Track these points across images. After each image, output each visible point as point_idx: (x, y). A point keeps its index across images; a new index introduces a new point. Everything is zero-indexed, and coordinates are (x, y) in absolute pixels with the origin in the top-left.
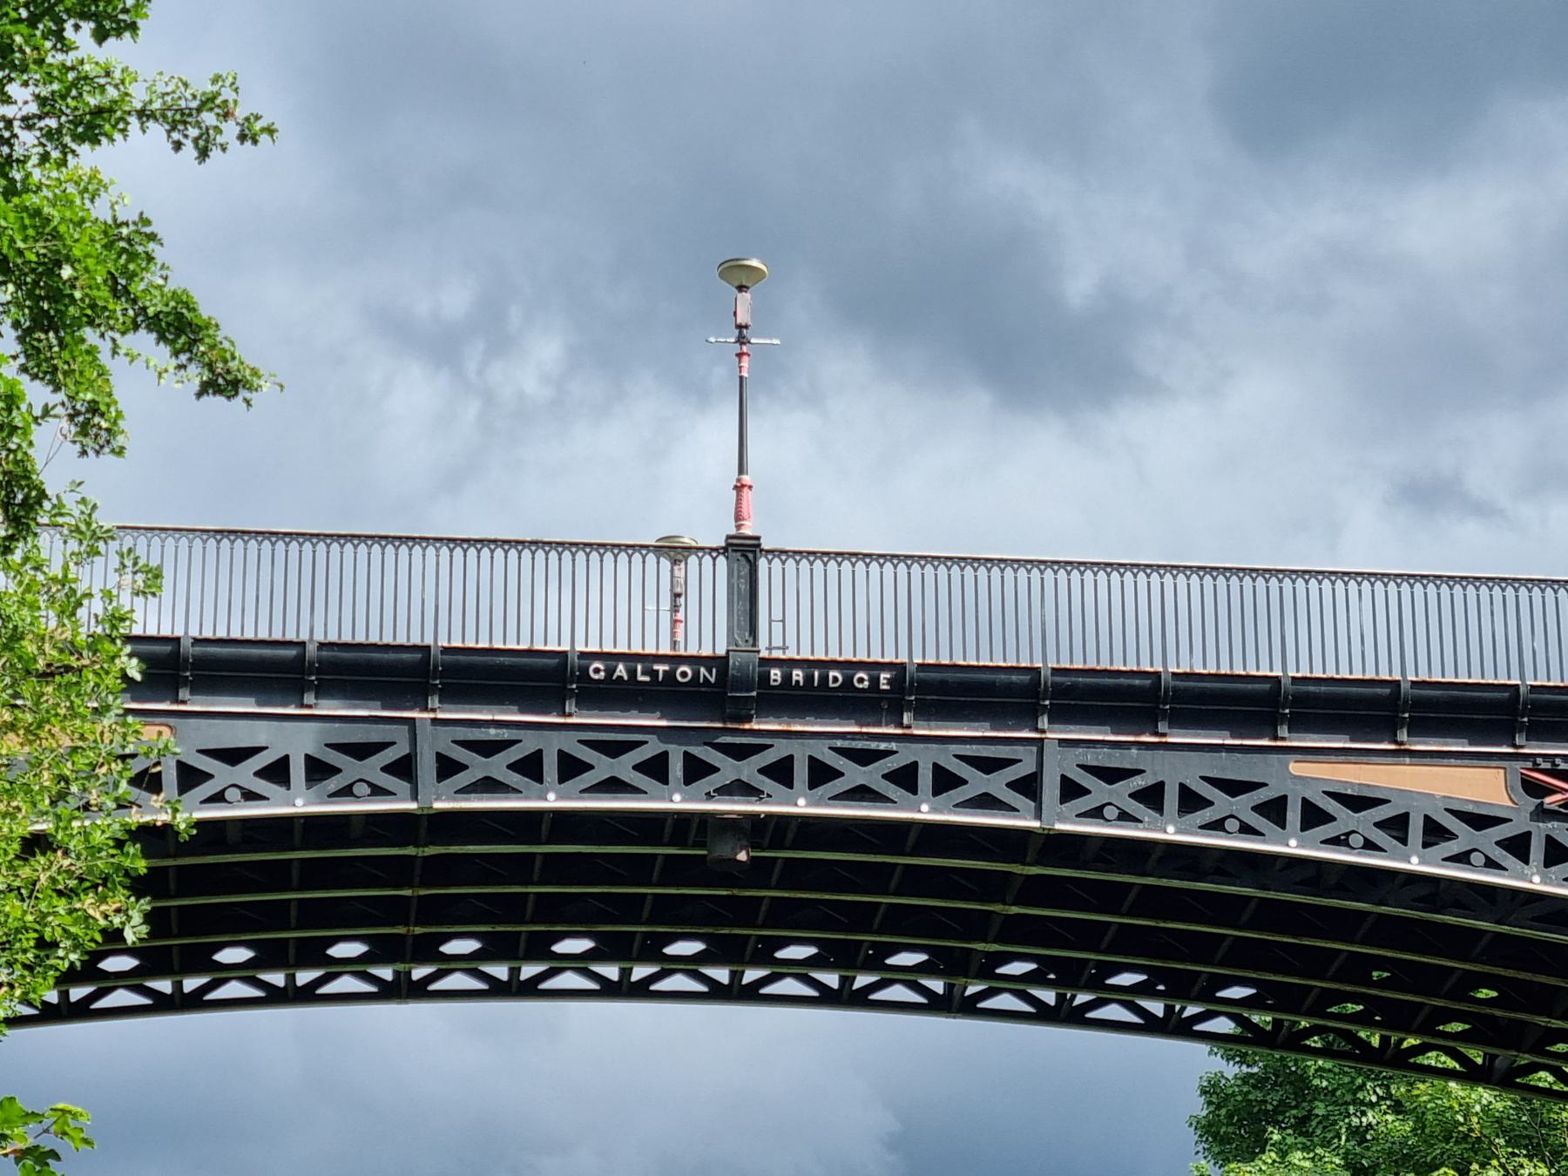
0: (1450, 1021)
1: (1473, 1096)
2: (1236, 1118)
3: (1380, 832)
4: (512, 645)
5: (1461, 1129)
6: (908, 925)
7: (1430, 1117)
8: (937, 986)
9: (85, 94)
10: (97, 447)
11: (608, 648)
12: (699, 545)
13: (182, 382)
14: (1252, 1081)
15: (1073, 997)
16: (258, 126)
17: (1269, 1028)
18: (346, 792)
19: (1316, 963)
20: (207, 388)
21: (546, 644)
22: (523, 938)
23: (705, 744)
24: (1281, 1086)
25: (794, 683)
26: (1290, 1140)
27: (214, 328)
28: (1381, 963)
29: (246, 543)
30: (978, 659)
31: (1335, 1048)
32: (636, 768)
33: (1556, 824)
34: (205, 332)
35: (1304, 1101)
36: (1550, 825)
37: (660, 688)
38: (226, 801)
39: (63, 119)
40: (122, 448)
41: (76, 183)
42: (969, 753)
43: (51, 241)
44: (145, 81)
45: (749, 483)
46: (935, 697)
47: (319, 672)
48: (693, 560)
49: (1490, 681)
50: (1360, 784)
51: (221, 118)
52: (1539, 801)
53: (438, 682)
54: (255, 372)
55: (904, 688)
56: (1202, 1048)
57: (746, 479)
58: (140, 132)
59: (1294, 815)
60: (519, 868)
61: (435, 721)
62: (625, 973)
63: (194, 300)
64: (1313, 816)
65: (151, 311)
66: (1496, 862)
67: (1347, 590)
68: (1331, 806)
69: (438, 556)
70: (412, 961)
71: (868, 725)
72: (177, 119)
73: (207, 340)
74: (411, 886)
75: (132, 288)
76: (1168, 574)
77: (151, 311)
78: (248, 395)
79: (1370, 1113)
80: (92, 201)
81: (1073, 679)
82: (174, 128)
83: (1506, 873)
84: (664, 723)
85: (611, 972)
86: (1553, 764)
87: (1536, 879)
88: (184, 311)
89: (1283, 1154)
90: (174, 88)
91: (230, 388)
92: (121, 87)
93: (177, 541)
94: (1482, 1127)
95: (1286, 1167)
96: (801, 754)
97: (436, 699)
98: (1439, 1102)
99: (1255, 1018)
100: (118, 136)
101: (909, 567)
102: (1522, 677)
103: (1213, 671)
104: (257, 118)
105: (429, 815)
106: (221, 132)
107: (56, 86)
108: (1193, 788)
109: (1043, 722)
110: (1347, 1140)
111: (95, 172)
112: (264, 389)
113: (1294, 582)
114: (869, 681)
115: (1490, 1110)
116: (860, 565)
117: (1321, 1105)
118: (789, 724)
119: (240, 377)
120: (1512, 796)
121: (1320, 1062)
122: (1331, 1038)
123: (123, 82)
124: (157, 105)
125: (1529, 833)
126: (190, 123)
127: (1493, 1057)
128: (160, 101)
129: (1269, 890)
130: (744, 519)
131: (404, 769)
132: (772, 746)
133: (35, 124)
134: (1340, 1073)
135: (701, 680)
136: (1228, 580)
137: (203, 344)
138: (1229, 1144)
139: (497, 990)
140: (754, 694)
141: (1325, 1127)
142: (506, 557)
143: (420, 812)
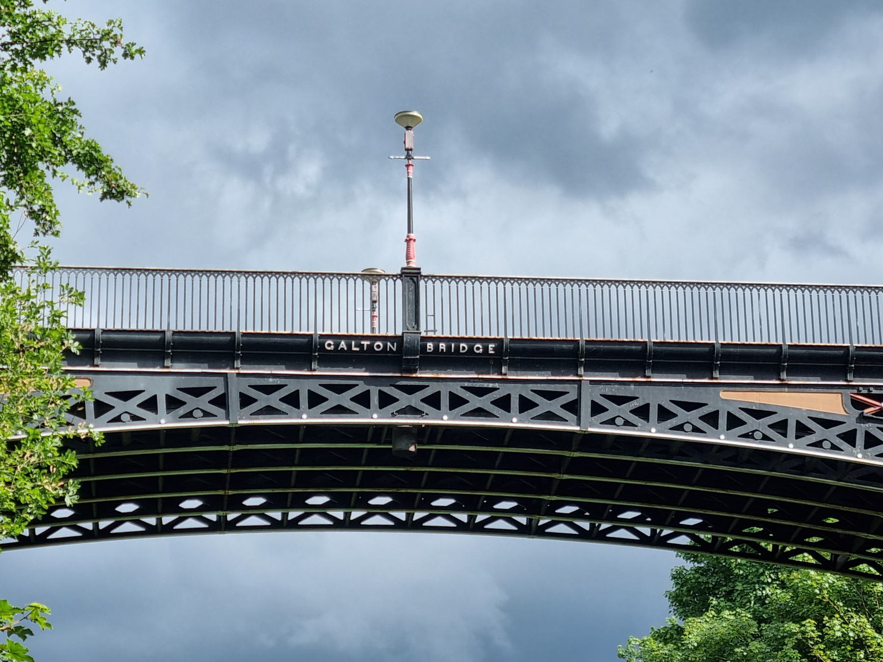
0: (812, 536)
1: (824, 579)
2: (692, 592)
3: (772, 430)
4: (281, 331)
5: (817, 597)
6: (506, 486)
7: (800, 590)
8: (523, 520)
9: (37, 31)
10: (44, 231)
11: (335, 332)
12: (386, 273)
13: (92, 192)
14: (700, 571)
15: (600, 525)
16: (134, 49)
17: (710, 541)
18: (189, 415)
19: (736, 504)
20: (104, 196)
21: (300, 330)
22: (290, 495)
23: (391, 385)
24: (717, 574)
25: (440, 351)
26: (722, 604)
27: (110, 162)
28: (773, 504)
29: (131, 275)
30: (544, 336)
31: (747, 552)
32: (352, 399)
33: (871, 424)
34: (105, 164)
35: (730, 582)
36: (867, 425)
37: (364, 354)
38: (122, 421)
39: (25, 45)
40: (58, 232)
41: (32, 80)
42: (539, 389)
43: (18, 114)
44: (71, 23)
45: (414, 238)
46: (520, 358)
47: (173, 347)
48: (383, 281)
49: (833, 344)
50: (760, 404)
51: (113, 45)
52: (861, 411)
53: (240, 352)
54: (133, 187)
55: (502, 353)
56: (672, 553)
57: (412, 236)
58: (68, 52)
59: (723, 421)
60: (287, 457)
61: (238, 375)
62: (347, 515)
63: (99, 146)
64: (734, 422)
65: (75, 153)
66: (838, 447)
67: (766, 294)
68: (744, 416)
69: (239, 281)
70: (227, 510)
71: (482, 374)
72: (89, 45)
73: (106, 169)
74: (227, 468)
75: (64, 139)
76: (651, 286)
77: (75, 153)
78: (129, 199)
79: (767, 589)
80: (41, 89)
81: (597, 346)
82: (87, 50)
83: (843, 452)
84: (367, 374)
85: (339, 514)
86: (869, 390)
87: (860, 456)
88: (93, 152)
89: (719, 612)
90: (87, 27)
91: (119, 195)
92: (57, 27)
93: (92, 275)
94: (830, 596)
95: (720, 619)
96: (445, 391)
97: (239, 362)
98: (805, 582)
99: (702, 536)
100: (55, 54)
101: (504, 284)
102: (851, 342)
103: (677, 341)
104: (133, 44)
105: (236, 428)
106: (113, 52)
107: (20, 26)
108: (666, 407)
109: (581, 371)
110: (755, 604)
111: (42, 72)
112: (138, 196)
113: (721, 290)
114: (483, 348)
115: (834, 586)
116: (485, 283)
117: (740, 584)
118: (437, 374)
119: (125, 189)
120: (846, 409)
121: (739, 561)
122: (745, 547)
123: (58, 24)
124: (77, 37)
125: (856, 430)
126: (96, 47)
127: (837, 556)
128: (79, 35)
129: (709, 463)
130: (411, 259)
131: (221, 401)
132: (428, 386)
133: (9, 47)
134: (750, 566)
135: (388, 350)
136: (669, 288)
137: (104, 170)
138: (688, 607)
139: (276, 525)
140: (418, 357)
141: (742, 597)
142: (277, 282)
143: (231, 426)
